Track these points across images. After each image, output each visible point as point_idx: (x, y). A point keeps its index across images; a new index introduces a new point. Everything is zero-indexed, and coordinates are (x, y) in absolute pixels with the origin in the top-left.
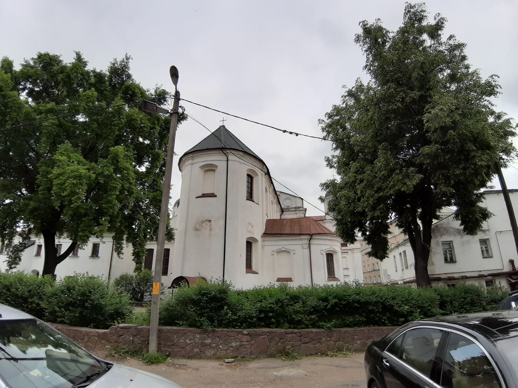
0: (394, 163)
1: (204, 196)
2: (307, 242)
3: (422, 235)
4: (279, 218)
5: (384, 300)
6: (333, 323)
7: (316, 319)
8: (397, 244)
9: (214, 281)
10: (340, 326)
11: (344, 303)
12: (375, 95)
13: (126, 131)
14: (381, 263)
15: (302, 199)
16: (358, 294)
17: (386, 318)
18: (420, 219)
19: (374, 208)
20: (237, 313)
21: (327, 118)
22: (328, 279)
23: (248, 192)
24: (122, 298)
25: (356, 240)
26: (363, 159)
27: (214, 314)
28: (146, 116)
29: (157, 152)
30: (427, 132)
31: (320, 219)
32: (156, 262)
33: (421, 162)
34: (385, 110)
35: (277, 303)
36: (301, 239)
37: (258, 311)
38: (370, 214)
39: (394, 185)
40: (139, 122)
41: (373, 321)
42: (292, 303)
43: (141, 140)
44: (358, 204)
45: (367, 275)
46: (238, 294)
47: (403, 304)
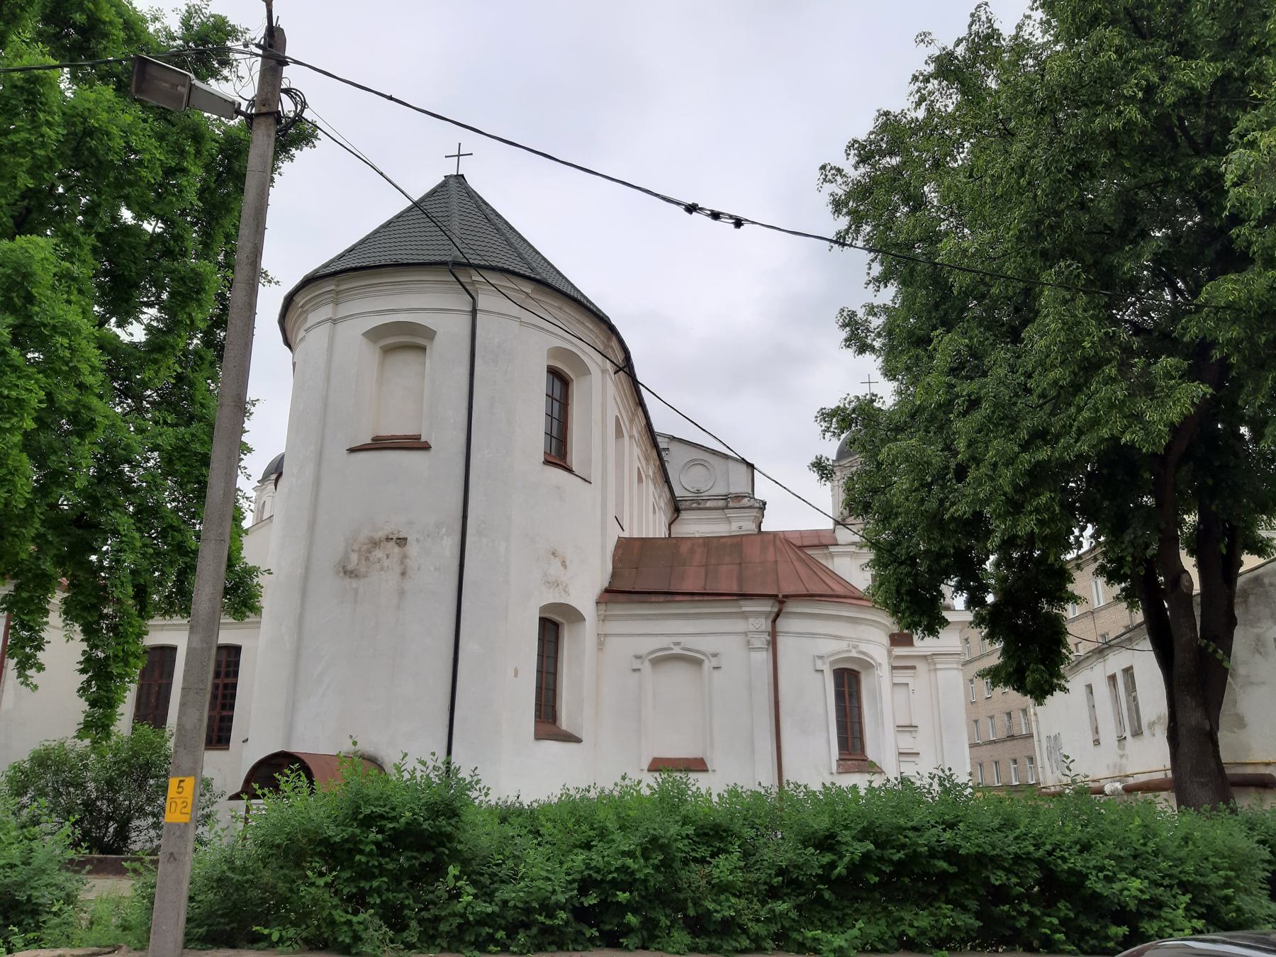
0: (1100, 339)
1: (380, 444)
2: (764, 624)
3: (1197, 612)
4: (661, 532)
5: (1050, 853)
6: (855, 932)
7: (794, 914)
8: (1100, 640)
9: (410, 768)
10: (880, 946)
11: (896, 857)
12: (1043, 76)
13: (64, 178)
14: (1039, 709)
15: (751, 466)
16: (951, 826)
17: (1056, 921)
18: (1191, 553)
19: (1014, 507)
20: (497, 890)
21: (853, 160)
22: (839, 766)
23: (549, 434)
24: (34, 844)
25: (944, 622)
26: (980, 321)
27: (407, 898)
28: (145, 121)
29: (193, 270)
30: (1236, 220)
31: (816, 542)
32: (183, 696)
33: (1204, 338)
34: (1076, 137)
35: (646, 854)
36: (745, 616)
37: (576, 885)
38: (999, 529)
39: (1095, 423)
40: (118, 143)
41: (1008, 933)
42: (703, 851)
43: (127, 215)
44: (956, 490)
45: (985, 752)
46: (504, 820)
47: (1123, 869)
